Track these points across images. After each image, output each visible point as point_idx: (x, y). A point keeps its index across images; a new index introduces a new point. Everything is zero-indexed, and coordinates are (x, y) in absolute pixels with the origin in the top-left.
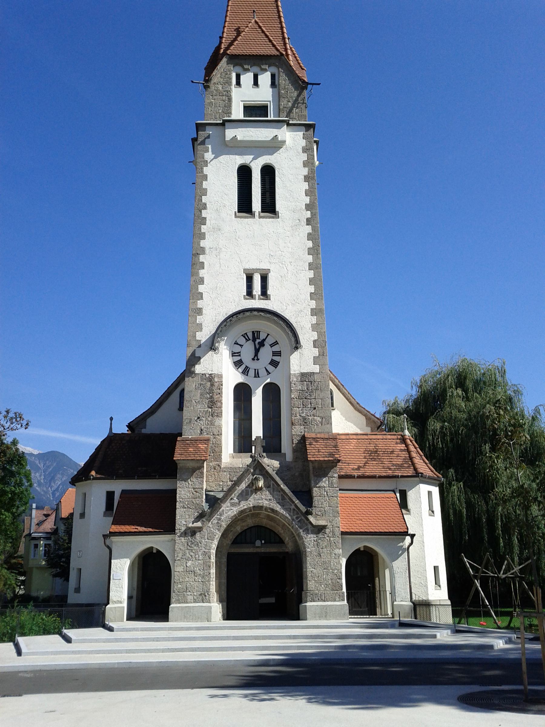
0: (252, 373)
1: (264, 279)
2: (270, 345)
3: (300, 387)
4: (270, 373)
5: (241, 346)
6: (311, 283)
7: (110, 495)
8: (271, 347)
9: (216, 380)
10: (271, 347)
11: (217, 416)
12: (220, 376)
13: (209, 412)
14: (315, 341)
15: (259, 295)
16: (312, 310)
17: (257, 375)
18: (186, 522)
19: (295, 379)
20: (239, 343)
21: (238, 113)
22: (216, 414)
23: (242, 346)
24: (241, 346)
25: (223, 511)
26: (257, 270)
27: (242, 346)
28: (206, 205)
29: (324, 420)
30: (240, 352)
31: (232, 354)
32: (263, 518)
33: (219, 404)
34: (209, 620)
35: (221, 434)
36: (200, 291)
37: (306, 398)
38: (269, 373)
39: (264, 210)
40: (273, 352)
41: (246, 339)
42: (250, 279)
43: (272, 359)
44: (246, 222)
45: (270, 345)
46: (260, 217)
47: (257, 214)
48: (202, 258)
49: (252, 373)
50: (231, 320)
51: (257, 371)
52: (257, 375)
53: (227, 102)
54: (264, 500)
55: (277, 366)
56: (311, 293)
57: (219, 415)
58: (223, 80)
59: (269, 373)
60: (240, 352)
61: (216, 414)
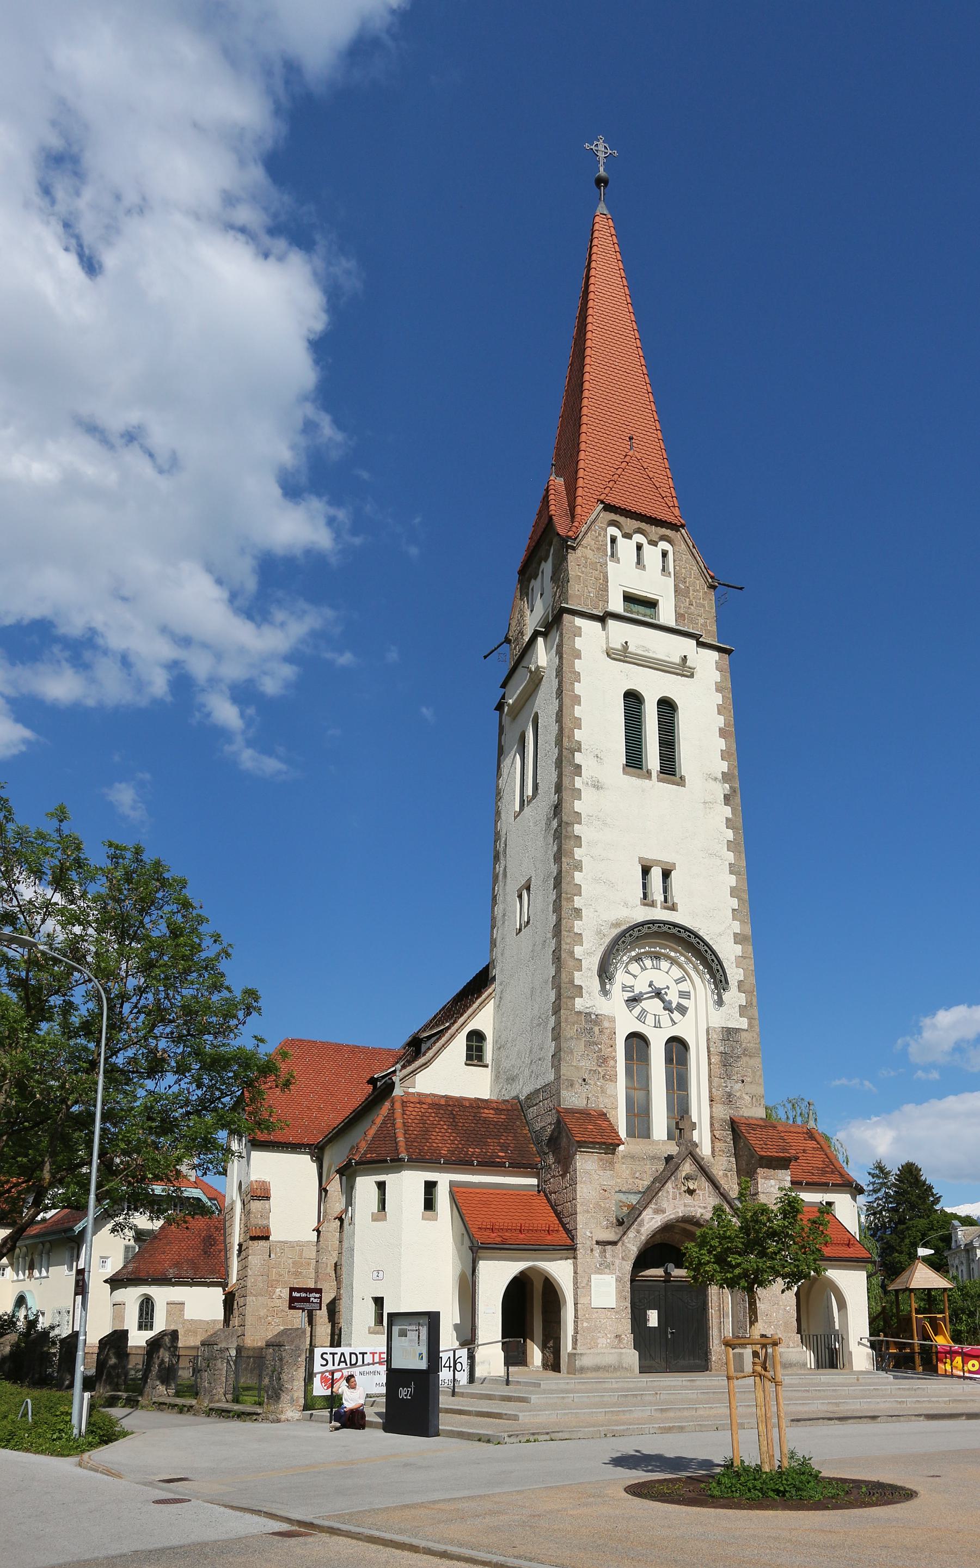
0: (650, 1020)
1: (666, 874)
2: (675, 981)
3: (722, 1048)
4: (676, 1023)
5: (635, 976)
6: (733, 894)
7: (430, 1187)
8: (677, 984)
9: (606, 1024)
10: (677, 984)
11: (611, 1081)
12: (612, 1020)
13: (599, 1073)
14: (740, 982)
15: (661, 902)
16: (735, 935)
17: (658, 1025)
18: (591, 1233)
19: (715, 1036)
20: (632, 972)
21: (616, 604)
22: (608, 1077)
23: (637, 976)
24: (635, 976)
25: (643, 1220)
26: (658, 863)
27: (637, 976)
28: (581, 745)
29: (754, 1098)
30: (633, 986)
31: (623, 988)
32: (677, 1233)
33: (612, 1063)
34: (743, 1371)
35: (617, 1108)
36: (577, 881)
37: (730, 1066)
38: (674, 1023)
39: (663, 771)
40: (679, 991)
41: (642, 968)
42: (646, 871)
43: (678, 1003)
44: (633, 782)
45: (675, 981)
46: (659, 780)
47: (654, 774)
48: (577, 829)
49: (650, 1020)
50: (631, 935)
51: (657, 1017)
52: (658, 1025)
53: (601, 581)
54: (697, 1208)
55: (685, 1014)
56: (733, 910)
57: (613, 1078)
58: (595, 544)
59: (674, 1023)
60: (633, 986)
61: (608, 1077)
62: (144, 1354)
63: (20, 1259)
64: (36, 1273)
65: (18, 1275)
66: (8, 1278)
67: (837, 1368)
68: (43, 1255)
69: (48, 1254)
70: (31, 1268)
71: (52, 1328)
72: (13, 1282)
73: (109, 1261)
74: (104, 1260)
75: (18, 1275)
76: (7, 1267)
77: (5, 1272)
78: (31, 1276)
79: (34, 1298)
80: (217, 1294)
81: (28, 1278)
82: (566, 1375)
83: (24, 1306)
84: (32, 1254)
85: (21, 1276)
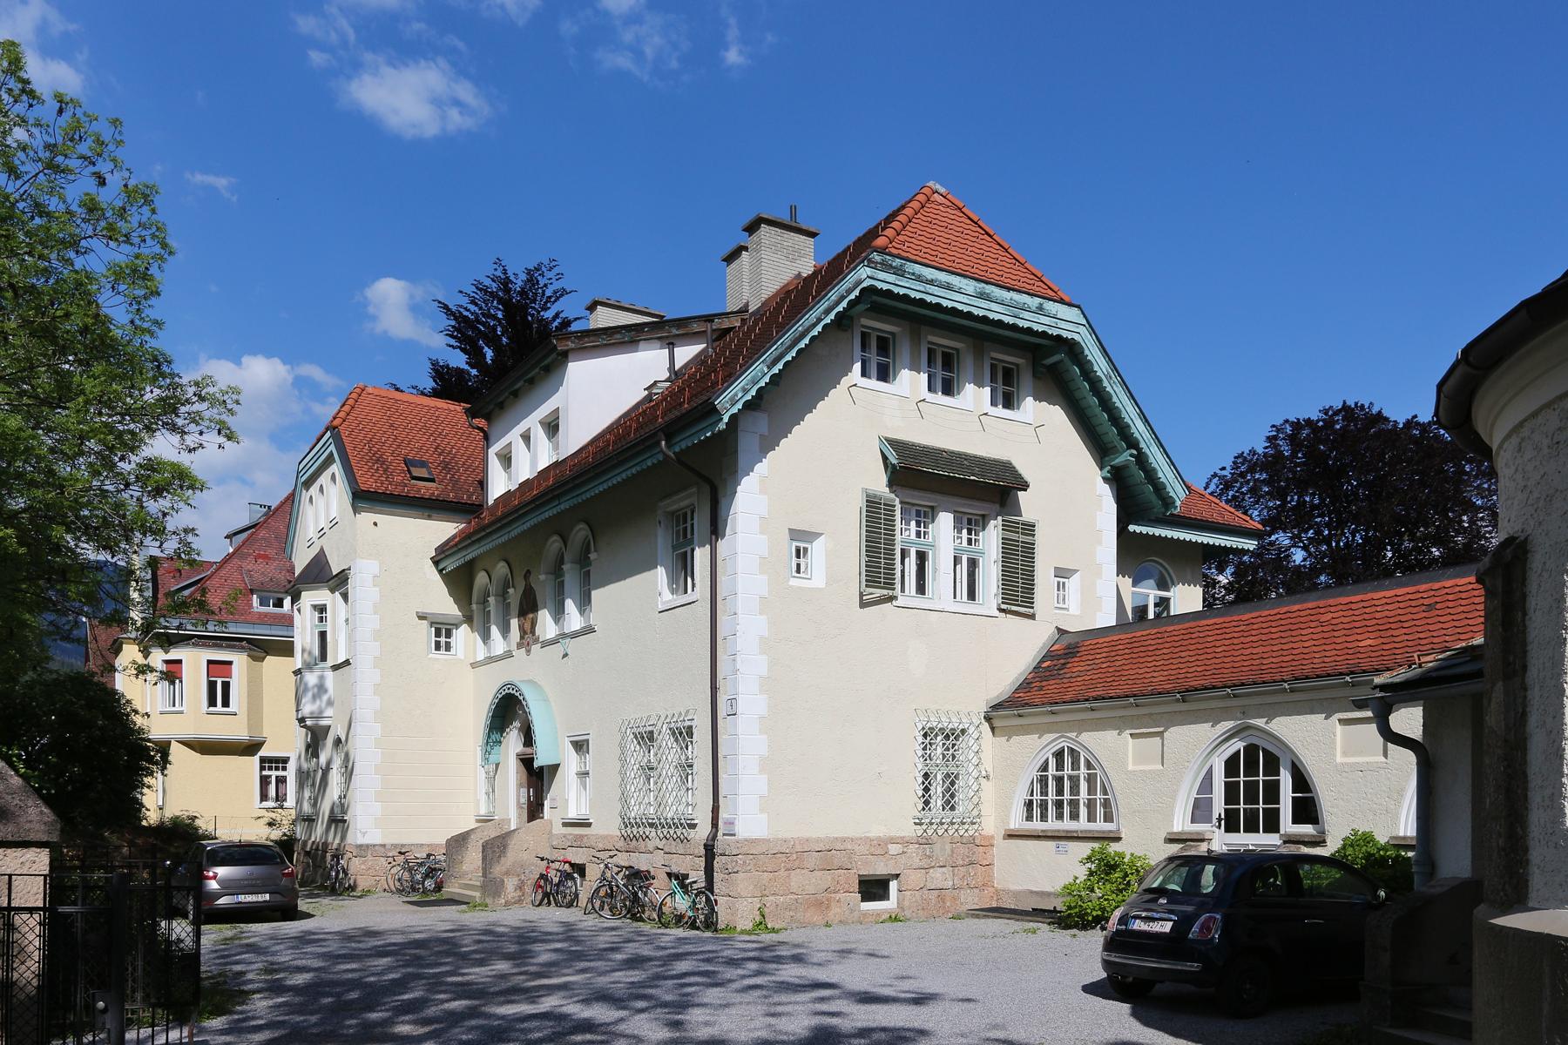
62: (45, 876)
63: (491, 599)
64: (546, 624)
65: (486, 637)
66: (461, 655)
67: (1096, 822)
68: (565, 567)
69: (583, 561)
70: (528, 607)
71: (149, 787)
72: (474, 665)
73: (817, 549)
74: (802, 545)
75: (486, 637)
76: (457, 626)
77: (452, 640)
78: (528, 635)
79: (546, 700)
80: (1463, 587)
81: (519, 646)
82: (444, 652)
83: (517, 724)
84: (528, 574)
85: (498, 644)
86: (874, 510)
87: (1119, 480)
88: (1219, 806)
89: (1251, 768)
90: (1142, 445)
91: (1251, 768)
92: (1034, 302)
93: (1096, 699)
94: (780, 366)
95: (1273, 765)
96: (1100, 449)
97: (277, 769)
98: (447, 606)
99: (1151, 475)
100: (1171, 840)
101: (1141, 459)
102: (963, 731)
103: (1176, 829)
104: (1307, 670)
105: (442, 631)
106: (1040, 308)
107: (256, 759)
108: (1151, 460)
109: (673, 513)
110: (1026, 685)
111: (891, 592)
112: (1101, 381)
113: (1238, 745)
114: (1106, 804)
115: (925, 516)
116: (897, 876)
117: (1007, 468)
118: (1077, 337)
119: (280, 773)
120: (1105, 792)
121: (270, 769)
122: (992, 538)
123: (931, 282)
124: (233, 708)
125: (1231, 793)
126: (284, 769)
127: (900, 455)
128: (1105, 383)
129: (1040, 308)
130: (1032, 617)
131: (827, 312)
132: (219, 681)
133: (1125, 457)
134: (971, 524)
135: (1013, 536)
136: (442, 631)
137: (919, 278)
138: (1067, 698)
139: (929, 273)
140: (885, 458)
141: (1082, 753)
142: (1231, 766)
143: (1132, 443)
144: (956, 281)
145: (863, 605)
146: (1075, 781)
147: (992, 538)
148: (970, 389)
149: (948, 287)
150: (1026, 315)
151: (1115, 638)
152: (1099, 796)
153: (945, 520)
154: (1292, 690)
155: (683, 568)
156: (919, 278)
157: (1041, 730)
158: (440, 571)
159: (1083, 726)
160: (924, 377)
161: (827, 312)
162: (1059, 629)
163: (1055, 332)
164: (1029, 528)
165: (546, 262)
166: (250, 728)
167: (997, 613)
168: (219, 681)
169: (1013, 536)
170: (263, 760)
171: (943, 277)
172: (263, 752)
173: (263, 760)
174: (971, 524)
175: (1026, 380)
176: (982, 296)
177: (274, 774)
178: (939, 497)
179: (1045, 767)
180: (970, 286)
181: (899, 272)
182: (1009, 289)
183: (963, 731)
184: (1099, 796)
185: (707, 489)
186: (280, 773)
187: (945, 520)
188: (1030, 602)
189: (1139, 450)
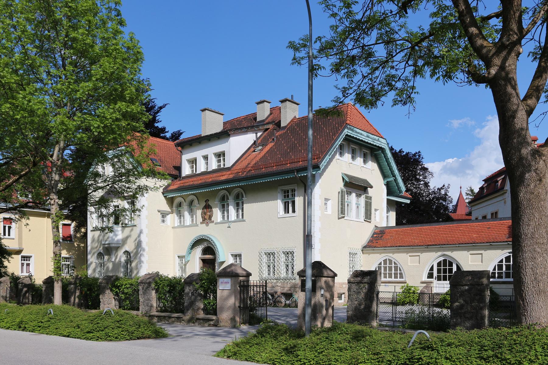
72: (173, 228)
73: (329, 203)
86: (342, 195)
87: (388, 185)
88: (435, 274)
89: (445, 265)
90: (397, 176)
91: (445, 265)
92: (377, 138)
93: (399, 246)
94: (331, 156)
95: (451, 264)
96: (385, 176)
97: (27, 260)
98: (166, 208)
99: (397, 184)
100: (422, 283)
101: (396, 180)
102: (356, 254)
103: (423, 280)
104: (461, 242)
105: (164, 215)
106: (378, 140)
107: (20, 256)
108: (398, 180)
109: (282, 190)
110: (370, 241)
111: (343, 216)
112: (389, 159)
113: (442, 259)
114: (401, 274)
115: (349, 193)
116: (344, 293)
117: (365, 181)
118: (385, 147)
119: (28, 262)
120: (400, 270)
121: (24, 260)
122: (362, 199)
123: (358, 133)
124: (12, 236)
125: (439, 271)
126: (29, 260)
127: (349, 179)
128: (390, 160)
129: (378, 140)
130: (370, 222)
131: (339, 141)
132: (7, 226)
133: (392, 179)
134: (359, 196)
135: (367, 200)
136: (164, 215)
137: (356, 132)
138: (389, 245)
139: (358, 131)
140: (343, 179)
141: (393, 261)
142: (439, 264)
143: (394, 176)
144: (363, 132)
145: (339, 219)
146: (390, 269)
147: (362, 199)
148: (359, 158)
149: (361, 134)
150: (375, 141)
151: (397, 229)
152: (399, 272)
153: (354, 195)
154: (458, 246)
155: (289, 206)
156: (356, 132)
157: (381, 253)
158: (165, 197)
159: (393, 253)
160: (362, 159)
161: (339, 141)
162: (376, 226)
163: (380, 146)
164: (370, 198)
165: (145, 79)
166: (19, 245)
167: (364, 221)
168: (7, 226)
169: (367, 200)
170: (22, 257)
171: (361, 131)
172: (23, 254)
173: (22, 257)
174: (359, 196)
175: (369, 157)
176: (368, 137)
177: (25, 262)
178: (353, 189)
179: (380, 264)
180: (365, 134)
181: (352, 130)
182: (373, 135)
183: (356, 254)
184: (399, 272)
185: (304, 185)
186: (28, 262)
187: (354, 195)
188: (370, 219)
189: (396, 178)
